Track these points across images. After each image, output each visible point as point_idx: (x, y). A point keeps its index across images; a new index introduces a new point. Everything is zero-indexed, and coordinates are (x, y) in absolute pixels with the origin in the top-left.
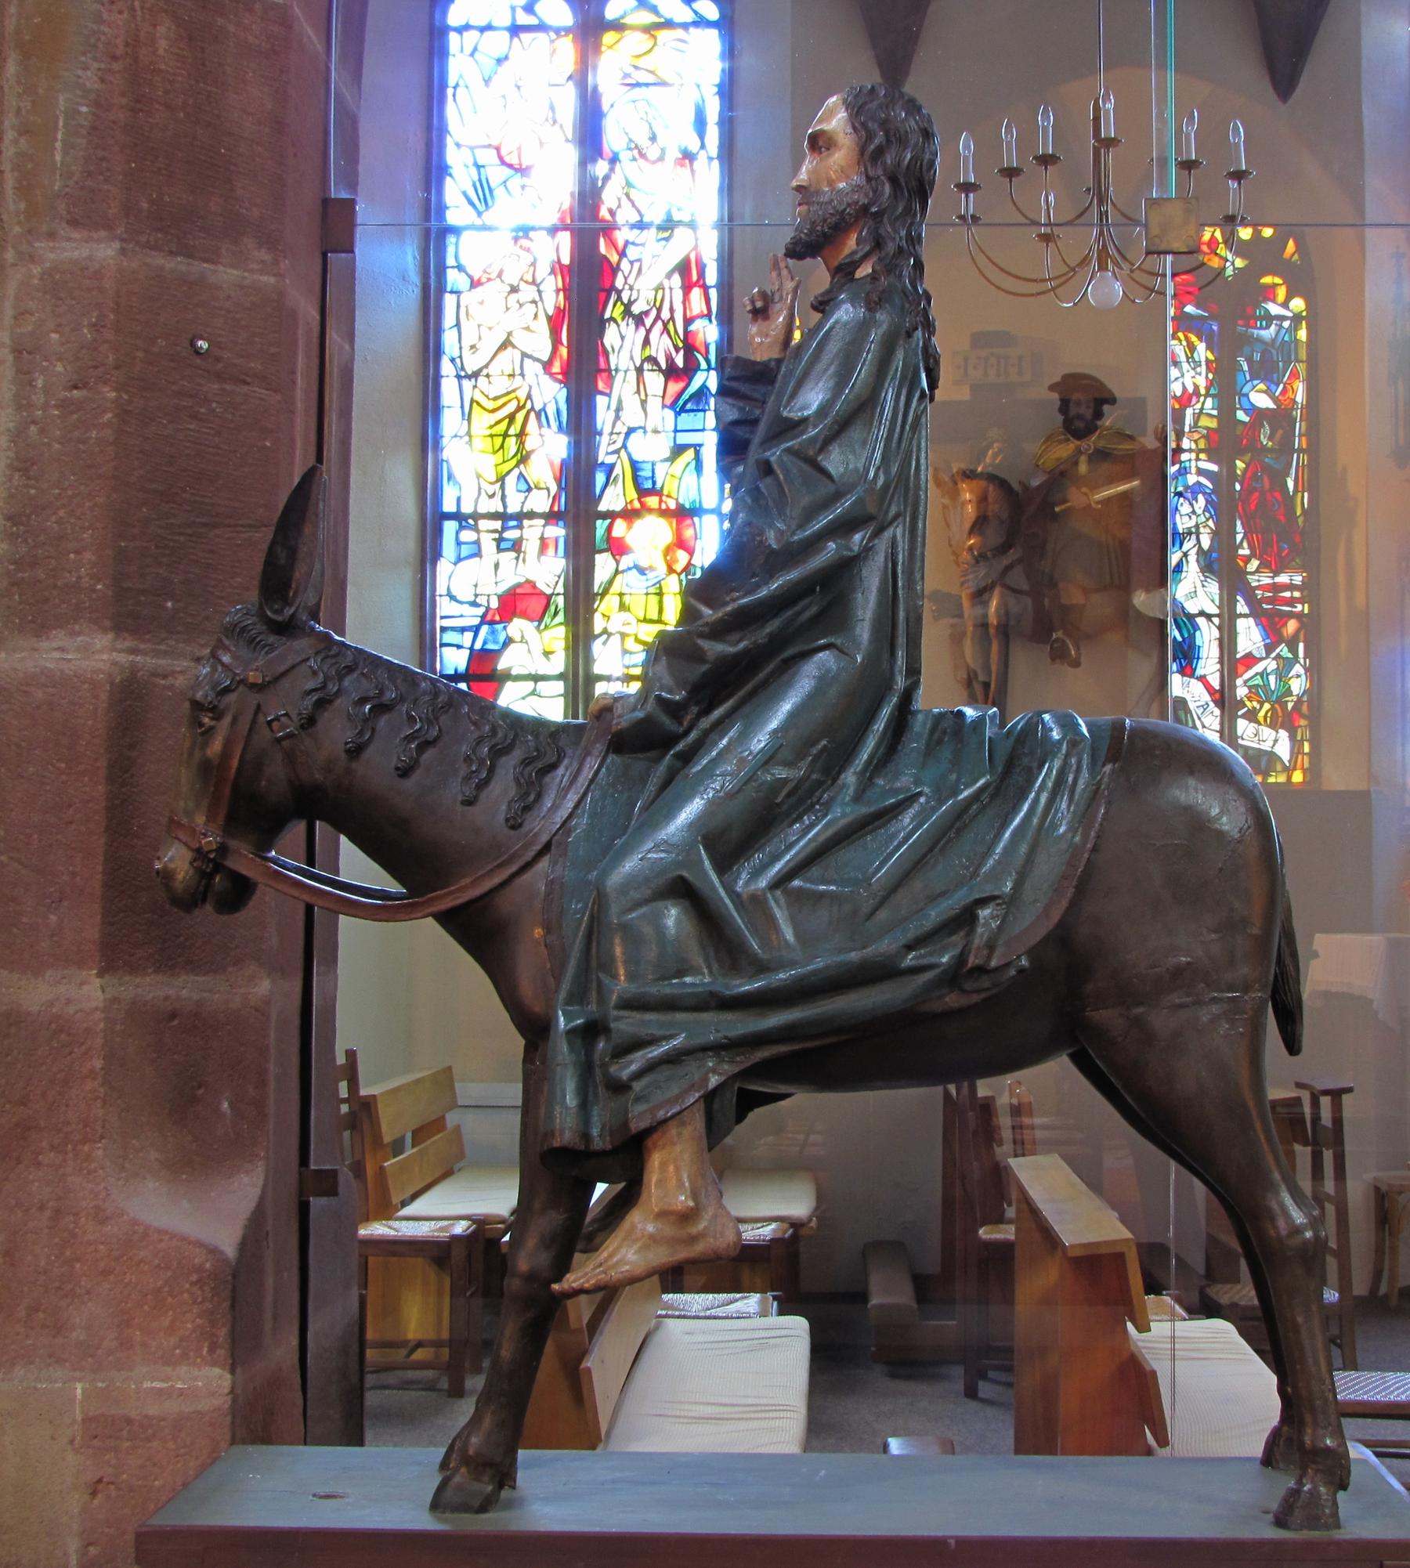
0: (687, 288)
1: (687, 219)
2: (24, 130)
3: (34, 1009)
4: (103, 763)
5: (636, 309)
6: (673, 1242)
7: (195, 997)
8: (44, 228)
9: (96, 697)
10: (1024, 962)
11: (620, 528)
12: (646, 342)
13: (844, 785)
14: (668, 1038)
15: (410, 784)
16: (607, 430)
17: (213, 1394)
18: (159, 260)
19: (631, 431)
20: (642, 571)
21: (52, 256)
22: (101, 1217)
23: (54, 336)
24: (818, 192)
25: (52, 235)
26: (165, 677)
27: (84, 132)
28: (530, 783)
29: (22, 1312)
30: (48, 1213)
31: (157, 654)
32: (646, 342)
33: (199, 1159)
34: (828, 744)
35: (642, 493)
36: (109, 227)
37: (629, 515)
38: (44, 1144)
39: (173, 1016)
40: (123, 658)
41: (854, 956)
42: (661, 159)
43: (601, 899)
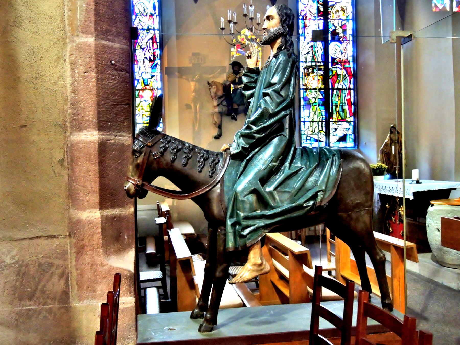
0: (153, 43)
1: (152, 28)
2: (70, 10)
3: (84, 219)
4: (97, 161)
5: (142, 47)
6: (257, 271)
7: (119, 213)
8: (76, 34)
9: (95, 146)
10: (327, 204)
11: (141, 93)
12: (145, 54)
13: (286, 166)
14: (254, 225)
15: (186, 168)
16: (137, 72)
17: (131, 303)
18: (103, 42)
19: (143, 72)
20: (146, 101)
21: (78, 41)
22: (102, 265)
23: (80, 60)
24: (269, 30)
25: (78, 36)
26: (109, 140)
27: (84, 11)
28: (214, 167)
29: (85, 288)
30: (90, 265)
31: (108, 135)
32: (145, 54)
33: (121, 250)
34: (282, 157)
35: (145, 85)
36: (92, 34)
37: (143, 90)
38: (88, 250)
39: (115, 218)
40: (101, 137)
41: (293, 205)
42: (147, 15)
43: (236, 193)
